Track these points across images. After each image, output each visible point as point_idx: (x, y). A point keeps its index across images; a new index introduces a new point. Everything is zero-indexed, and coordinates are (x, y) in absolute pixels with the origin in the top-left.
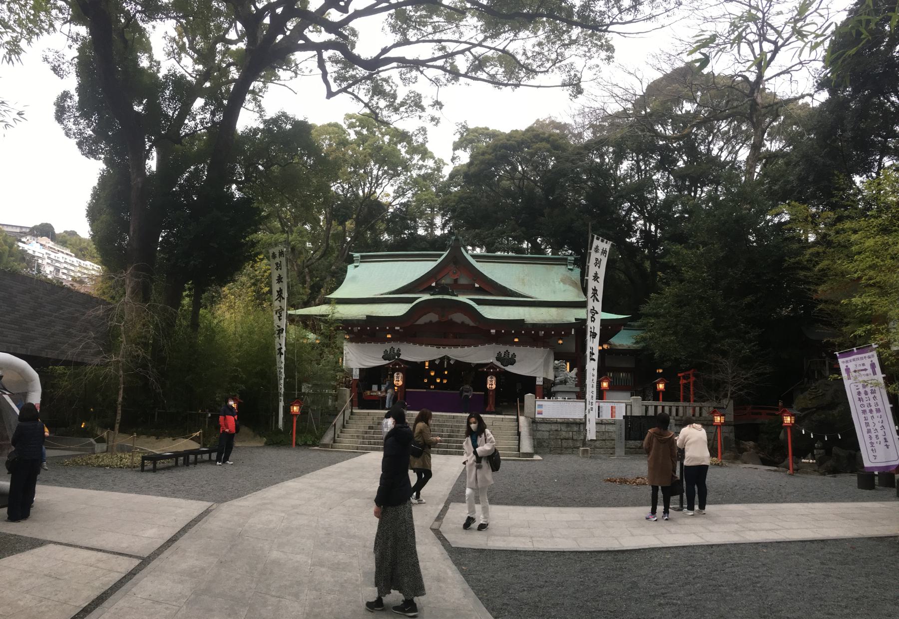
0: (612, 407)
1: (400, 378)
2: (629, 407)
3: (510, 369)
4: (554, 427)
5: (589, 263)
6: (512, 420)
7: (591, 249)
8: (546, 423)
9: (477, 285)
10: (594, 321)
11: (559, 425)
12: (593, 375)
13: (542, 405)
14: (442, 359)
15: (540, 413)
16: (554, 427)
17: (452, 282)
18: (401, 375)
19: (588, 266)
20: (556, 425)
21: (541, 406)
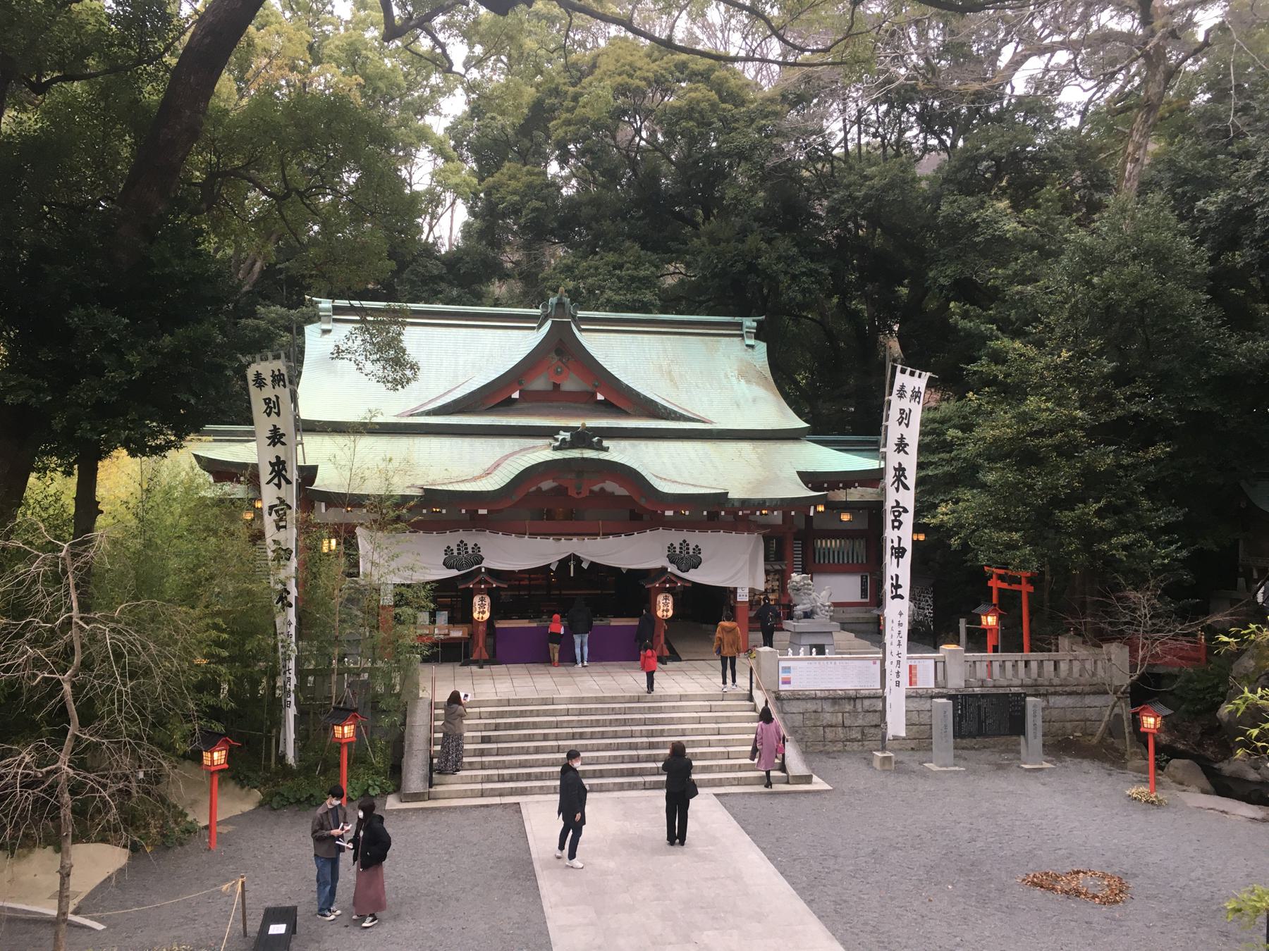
0: (910, 666)
2: (940, 665)
3: (694, 576)
4: (811, 706)
5: (887, 420)
6: (741, 697)
7: (890, 394)
8: (798, 699)
9: (600, 397)
10: (898, 528)
11: (819, 702)
12: (900, 625)
13: (789, 668)
14: (564, 563)
15: (787, 682)
16: (811, 706)
17: (550, 387)
19: (887, 427)
20: (814, 701)
21: (787, 669)
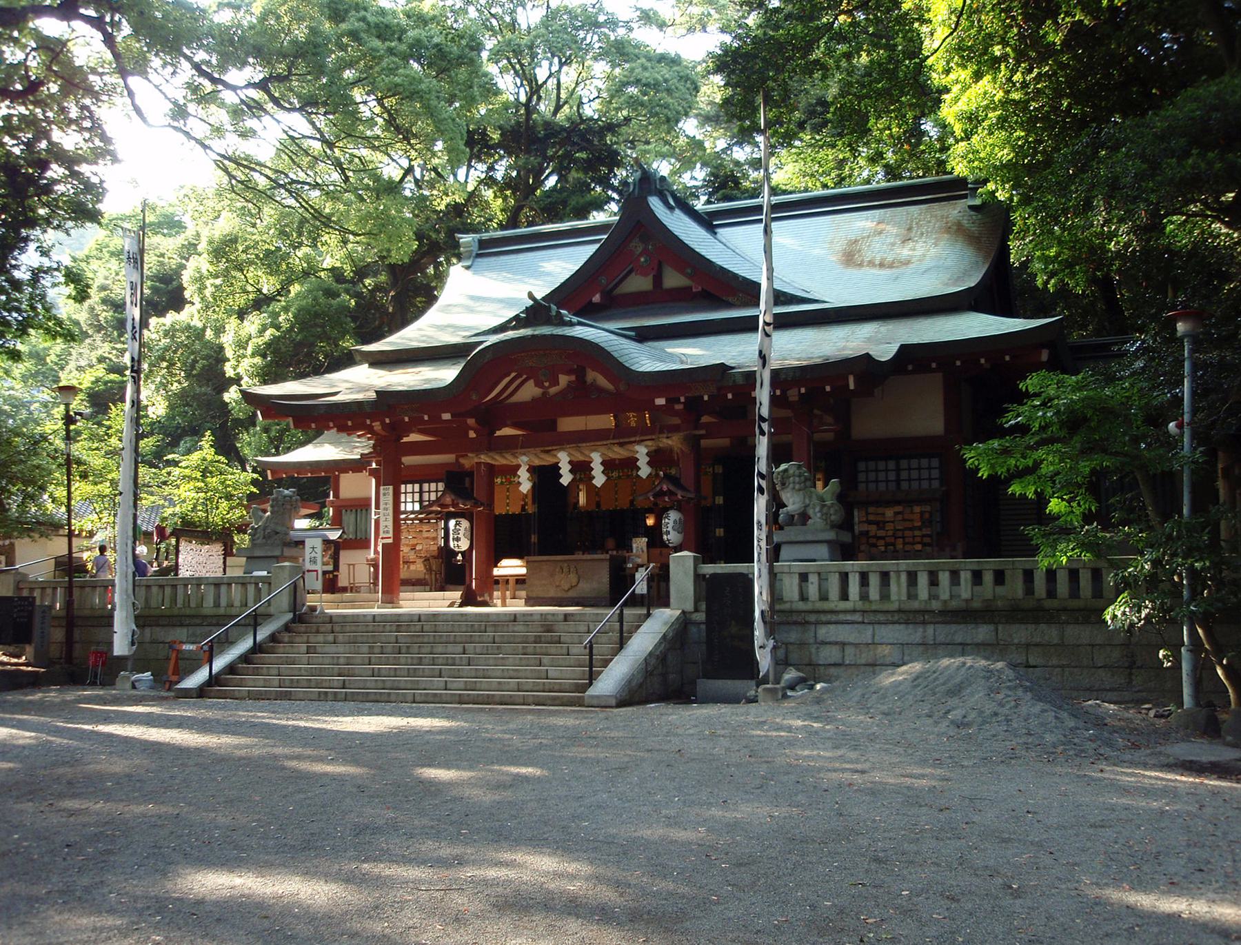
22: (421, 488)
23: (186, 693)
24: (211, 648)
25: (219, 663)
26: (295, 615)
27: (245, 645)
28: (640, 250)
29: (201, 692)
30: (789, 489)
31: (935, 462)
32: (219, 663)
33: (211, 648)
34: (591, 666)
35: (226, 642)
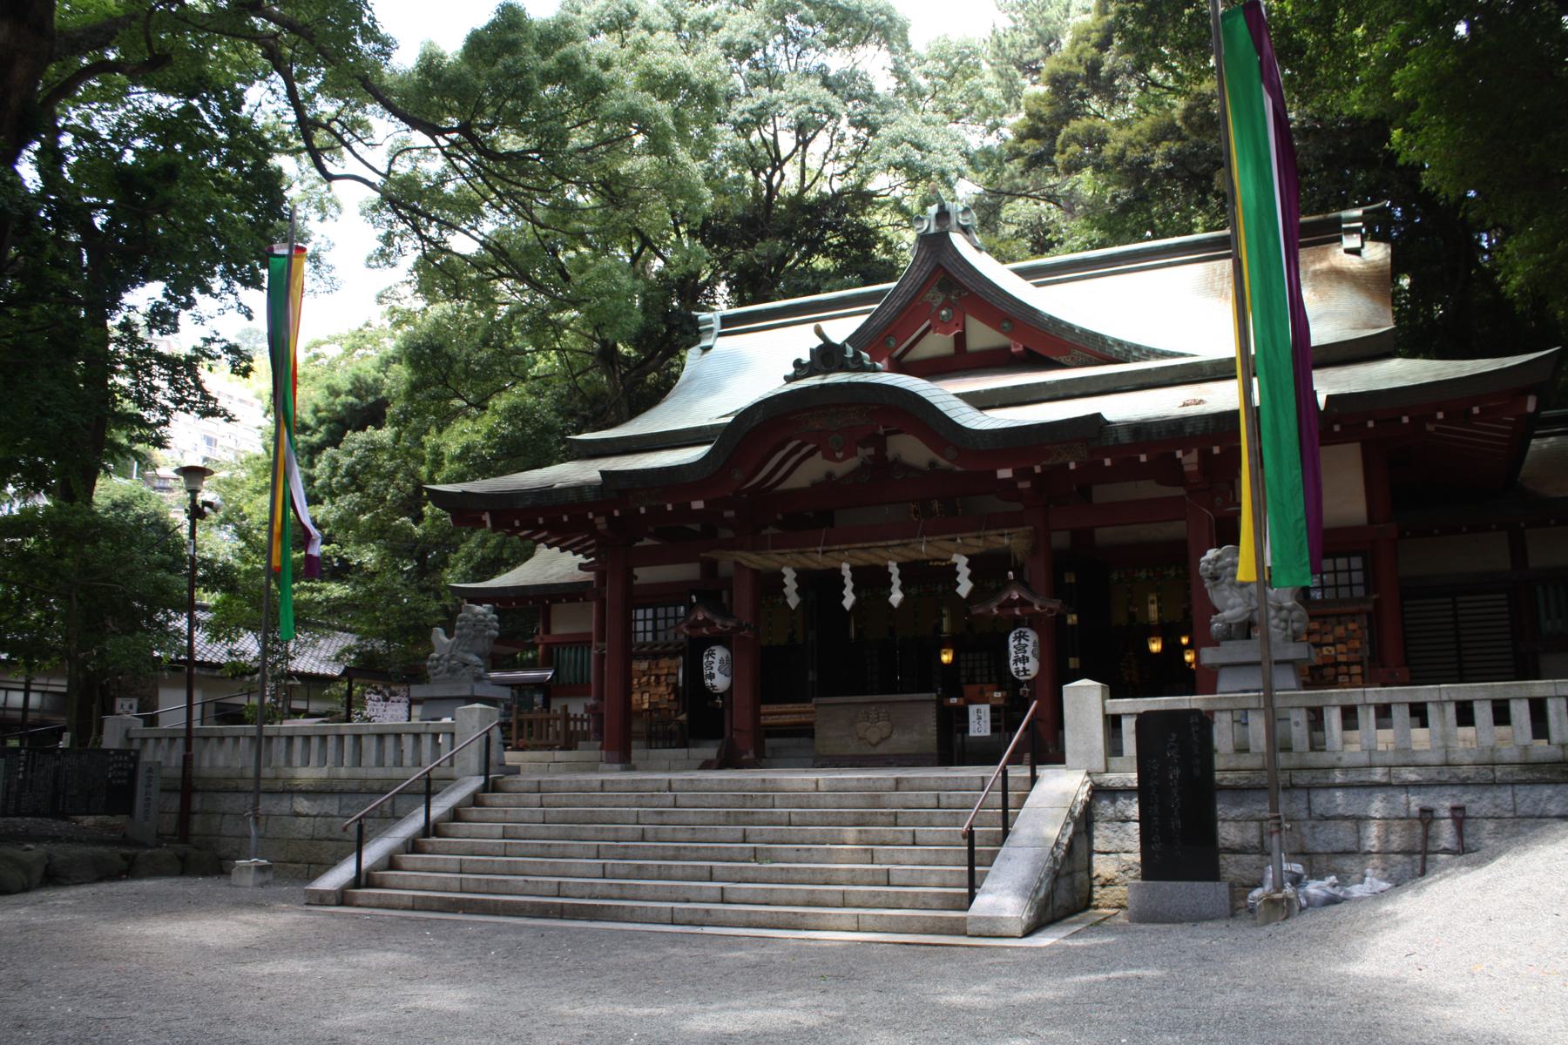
1: (1029, 649)
18: (1032, 637)
22: (655, 613)
23: (322, 899)
24: (360, 828)
25: (373, 852)
26: (487, 779)
27: (412, 825)
28: (940, 300)
29: (342, 897)
30: (1224, 586)
31: (1357, 562)
32: (373, 852)
33: (360, 828)
34: (971, 865)
35: (393, 817)
